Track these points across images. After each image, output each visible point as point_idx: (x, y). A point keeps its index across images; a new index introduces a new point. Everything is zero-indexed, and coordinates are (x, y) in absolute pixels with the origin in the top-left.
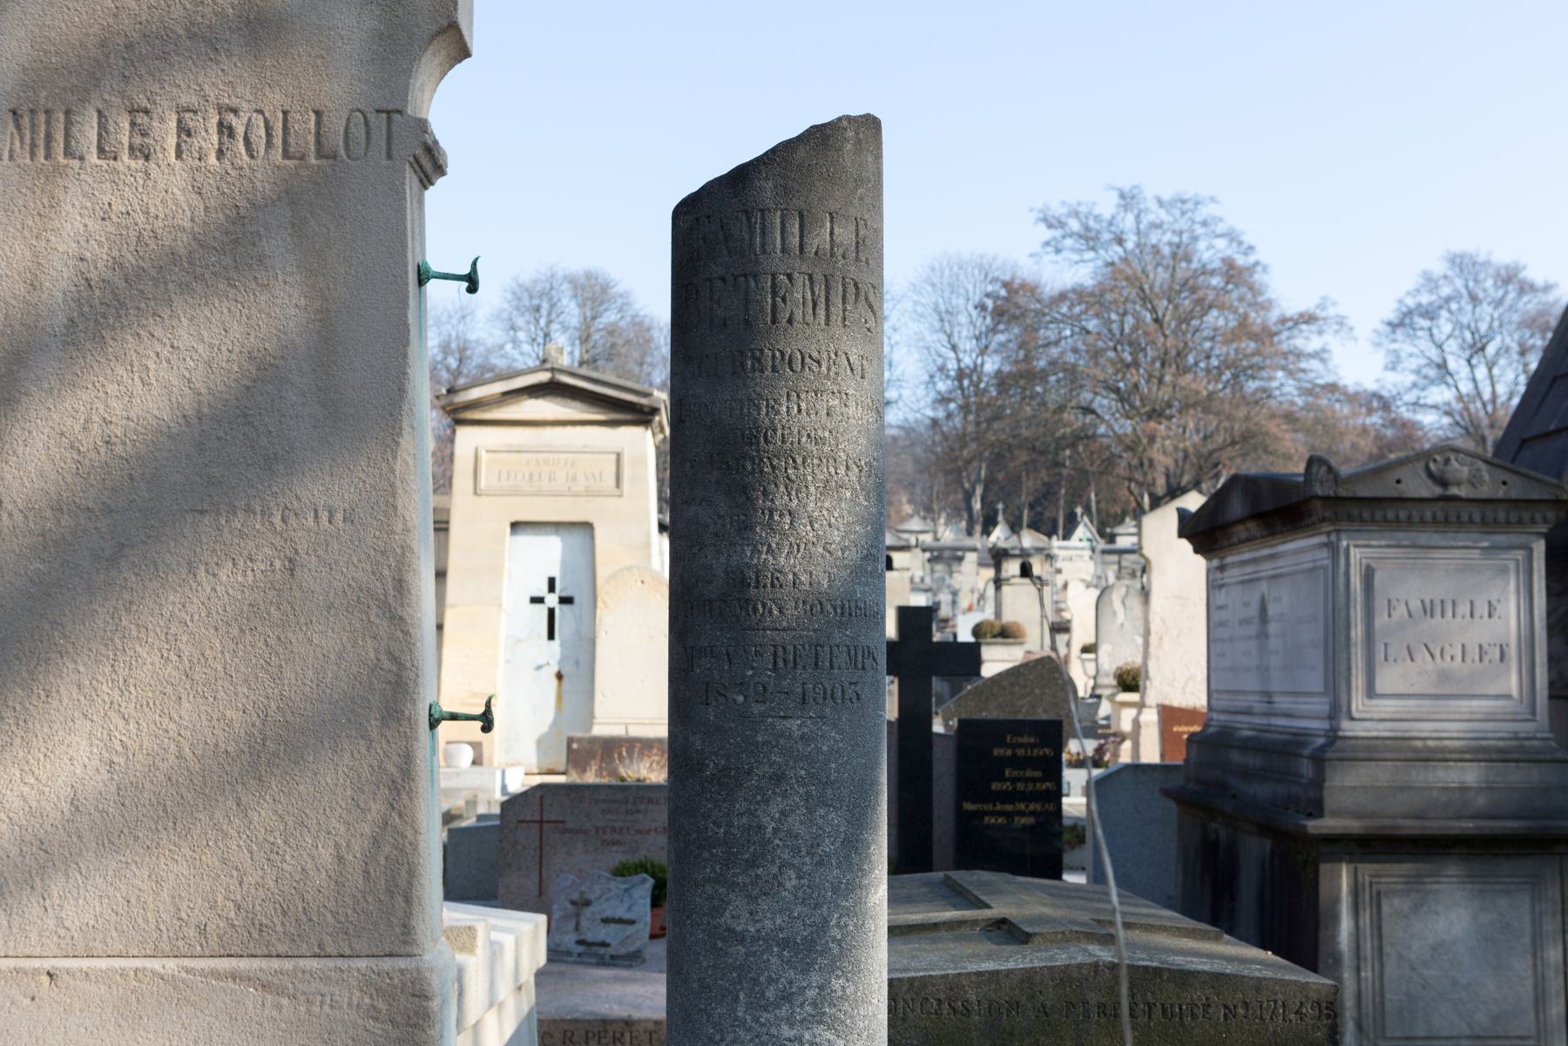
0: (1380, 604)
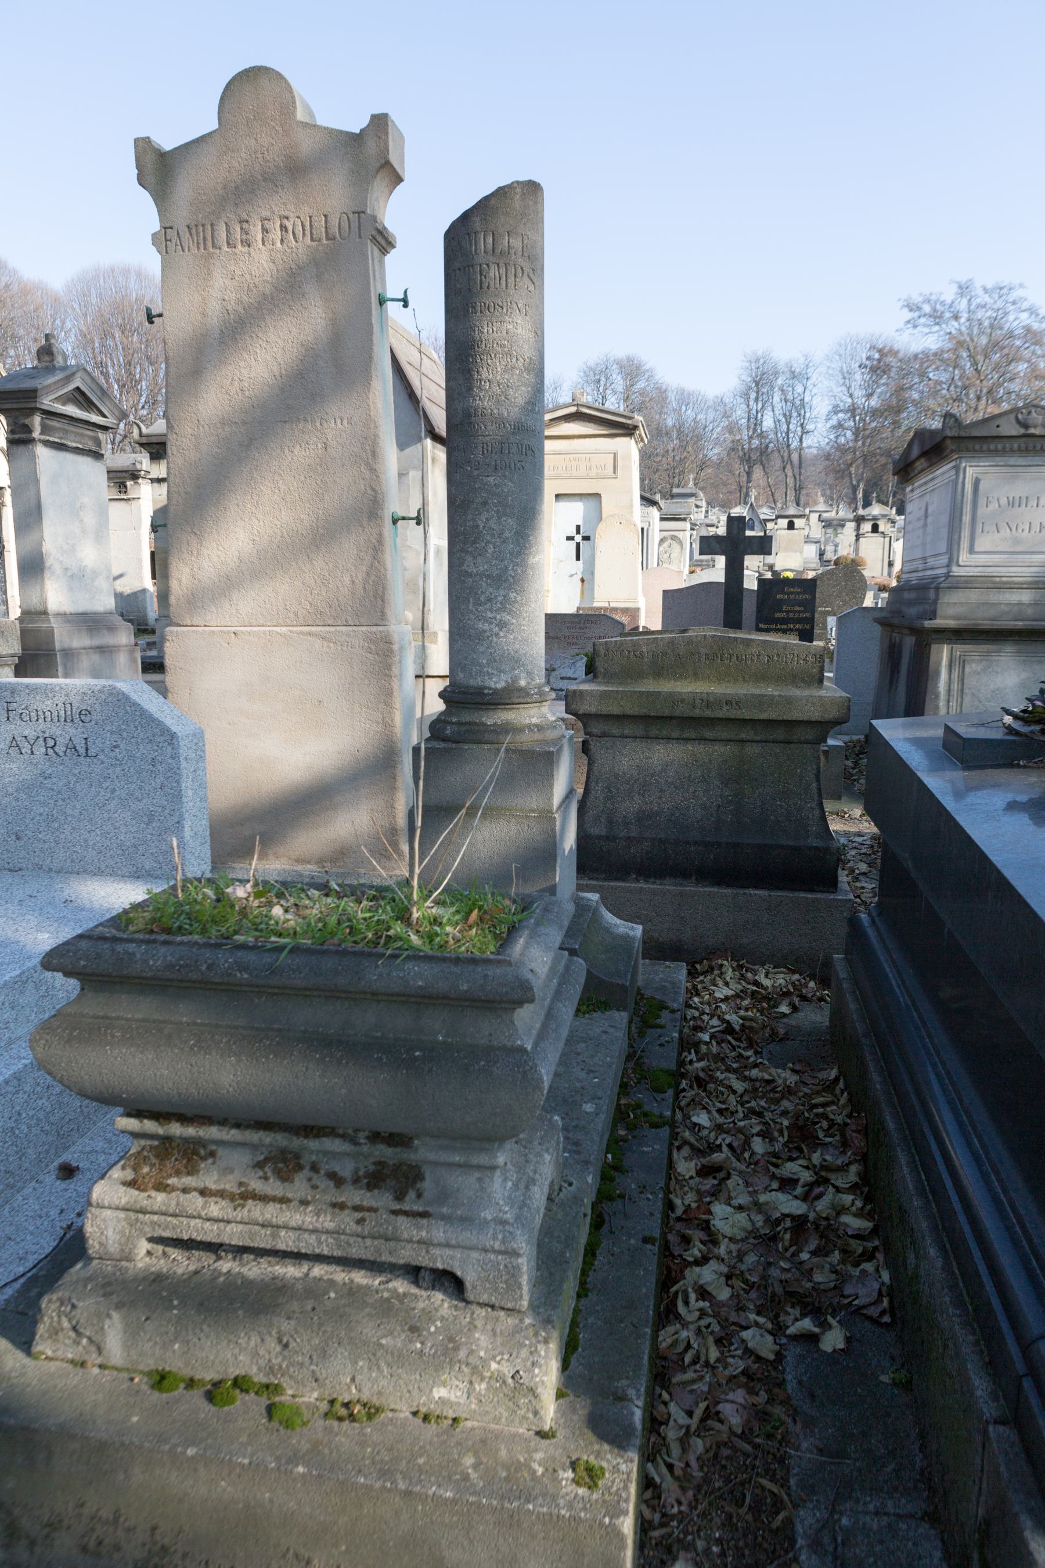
0: (982, 501)
